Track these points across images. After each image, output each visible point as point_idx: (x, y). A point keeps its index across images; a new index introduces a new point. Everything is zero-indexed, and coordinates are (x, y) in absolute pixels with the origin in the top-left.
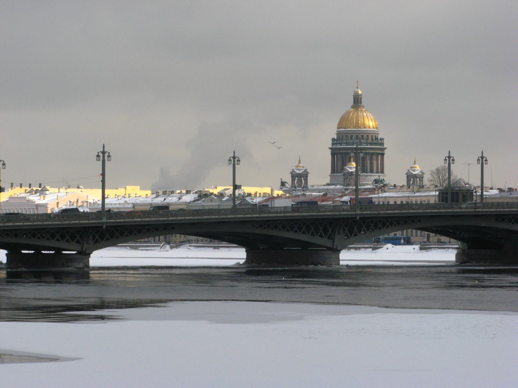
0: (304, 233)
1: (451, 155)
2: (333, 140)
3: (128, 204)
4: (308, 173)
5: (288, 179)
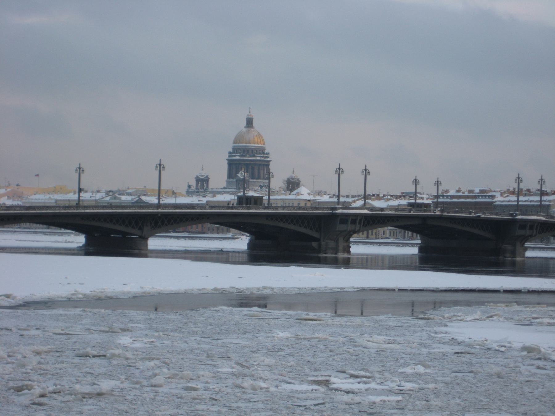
0: (120, 225)
1: (341, 167)
2: (230, 153)
3: (52, 199)
4: (209, 178)
5: (193, 183)
